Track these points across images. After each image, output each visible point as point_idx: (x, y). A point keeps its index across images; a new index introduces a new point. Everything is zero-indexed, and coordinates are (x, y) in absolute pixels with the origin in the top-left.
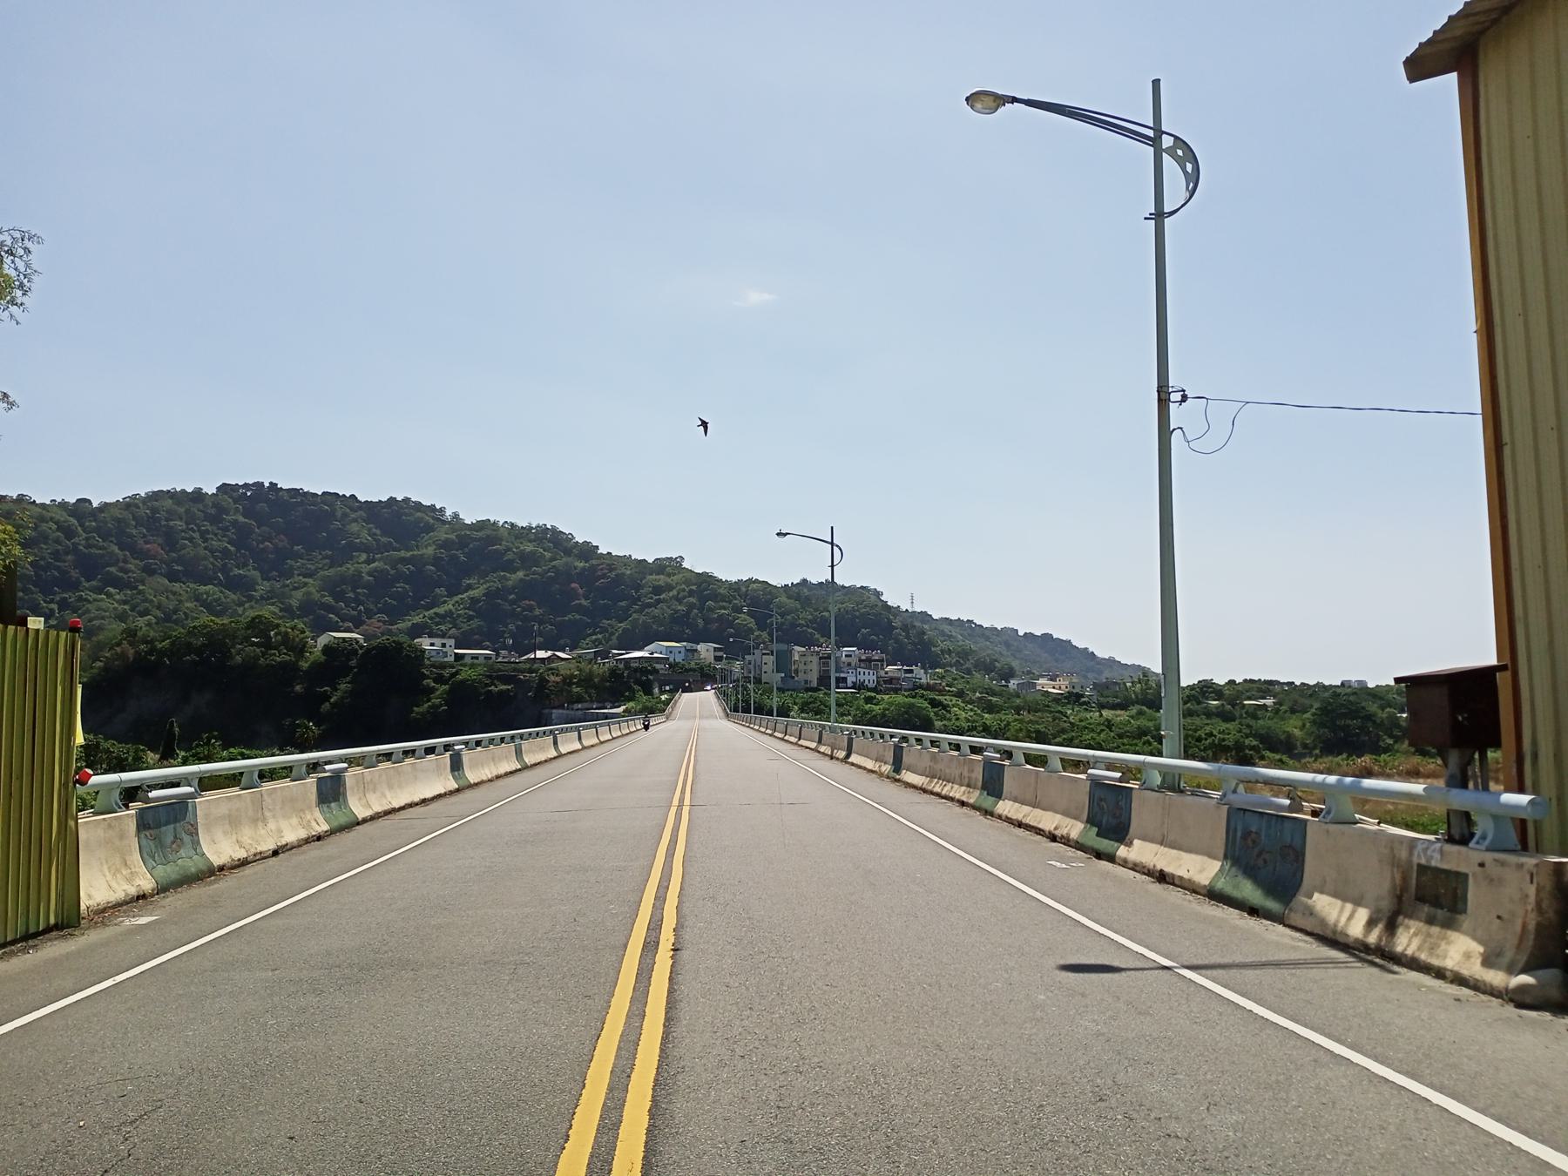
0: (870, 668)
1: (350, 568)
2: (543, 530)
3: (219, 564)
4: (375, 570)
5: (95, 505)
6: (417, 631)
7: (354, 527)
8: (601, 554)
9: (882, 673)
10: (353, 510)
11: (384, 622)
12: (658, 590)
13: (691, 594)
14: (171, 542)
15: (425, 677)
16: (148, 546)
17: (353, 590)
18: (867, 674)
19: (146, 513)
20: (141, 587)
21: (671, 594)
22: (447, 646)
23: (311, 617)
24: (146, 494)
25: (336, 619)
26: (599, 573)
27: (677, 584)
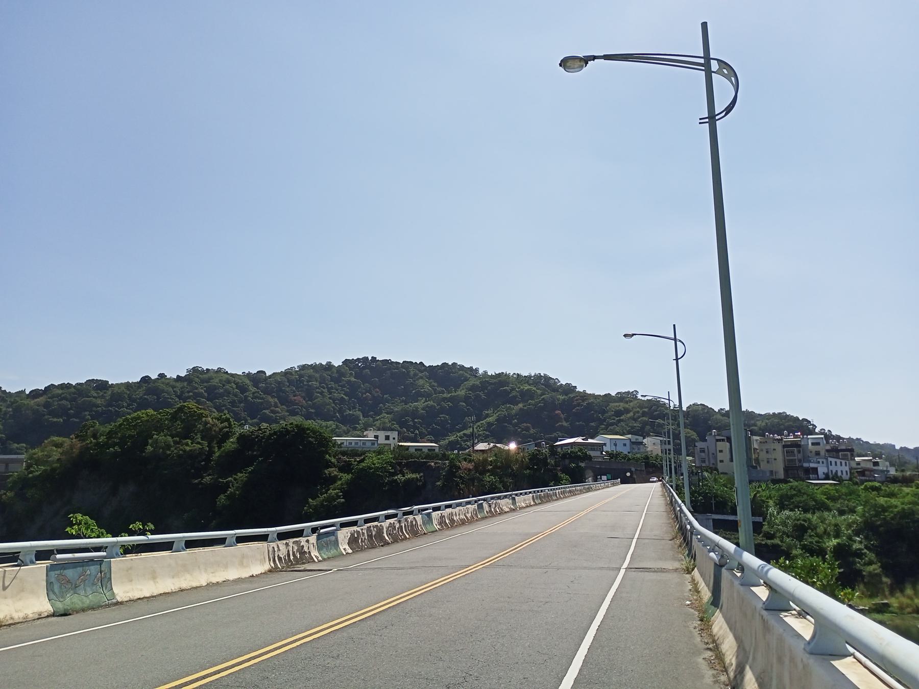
0: (838, 458)
2: (538, 377)
7: (421, 382)
8: (578, 391)
9: (854, 465)
12: (618, 413)
13: (644, 414)
15: (328, 465)
16: (295, 398)
18: (838, 463)
21: (629, 415)
22: (391, 438)
26: (575, 403)
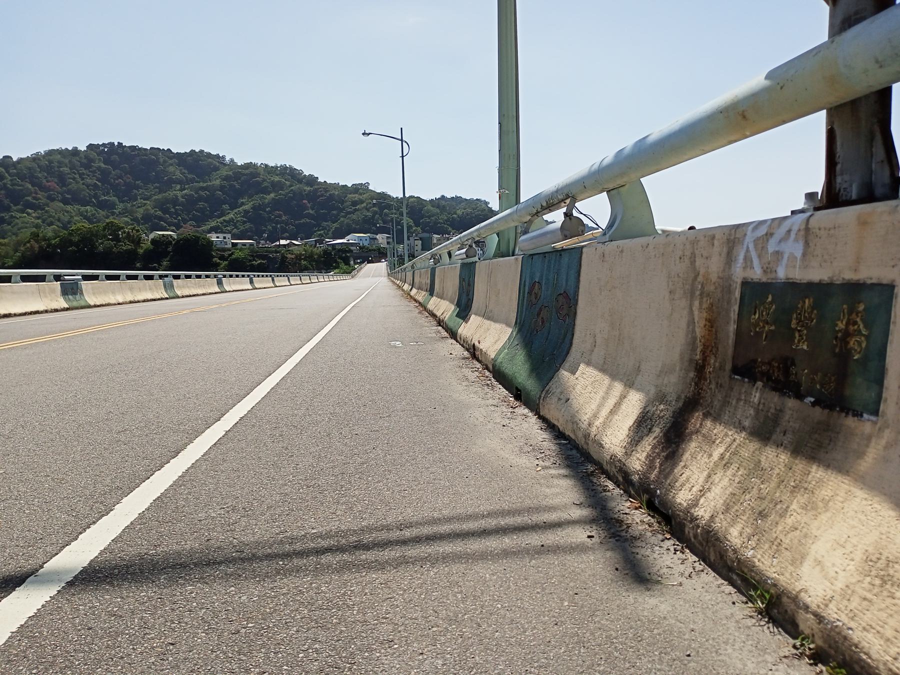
1: (170, 194)
2: (284, 168)
3: (92, 193)
4: (186, 195)
5: (15, 159)
6: (210, 231)
10: (171, 158)
11: (194, 226)
12: (354, 203)
14: (62, 180)
15: (214, 257)
16: (49, 183)
17: (174, 207)
19: (46, 164)
20: (47, 209)
22: (227, 238)
23: (150, 224)
24: (44, 152)
25: (165, 225)
27: (366, 199)
